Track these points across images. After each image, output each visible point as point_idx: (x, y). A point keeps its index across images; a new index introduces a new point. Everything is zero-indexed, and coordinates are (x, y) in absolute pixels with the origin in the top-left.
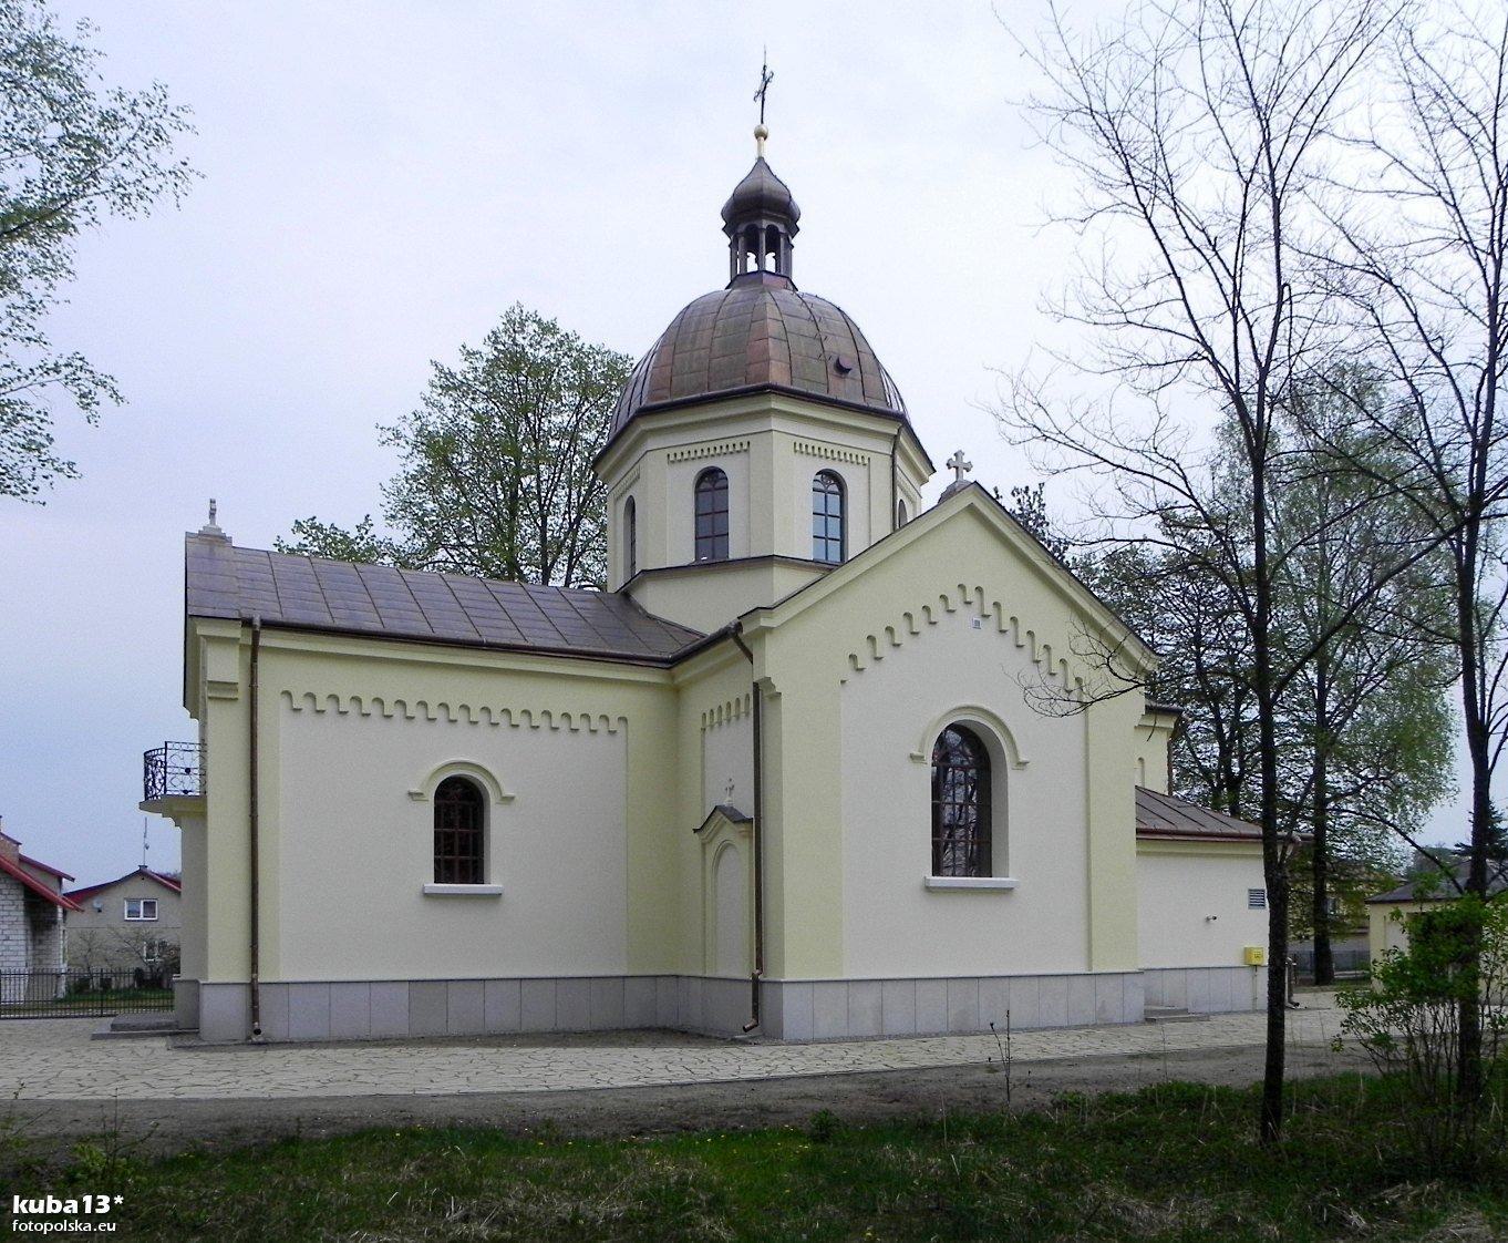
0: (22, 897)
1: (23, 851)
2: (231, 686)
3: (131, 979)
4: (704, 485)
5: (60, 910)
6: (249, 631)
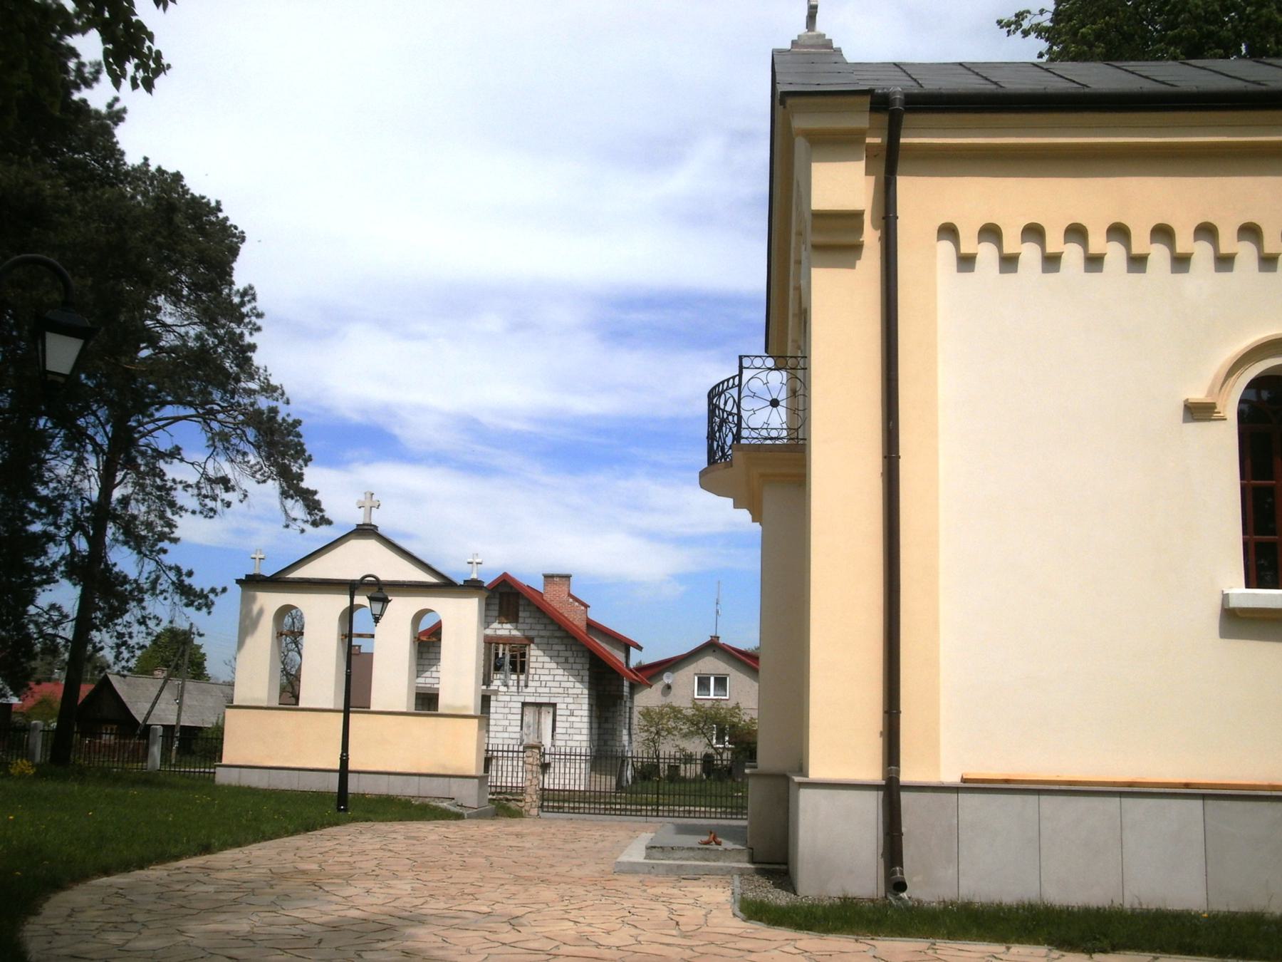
0: (587, 666)
1: (594, 615)
2: (854, 218)
3: (699, 767)
5: (626, 683)
6: (884, 119)
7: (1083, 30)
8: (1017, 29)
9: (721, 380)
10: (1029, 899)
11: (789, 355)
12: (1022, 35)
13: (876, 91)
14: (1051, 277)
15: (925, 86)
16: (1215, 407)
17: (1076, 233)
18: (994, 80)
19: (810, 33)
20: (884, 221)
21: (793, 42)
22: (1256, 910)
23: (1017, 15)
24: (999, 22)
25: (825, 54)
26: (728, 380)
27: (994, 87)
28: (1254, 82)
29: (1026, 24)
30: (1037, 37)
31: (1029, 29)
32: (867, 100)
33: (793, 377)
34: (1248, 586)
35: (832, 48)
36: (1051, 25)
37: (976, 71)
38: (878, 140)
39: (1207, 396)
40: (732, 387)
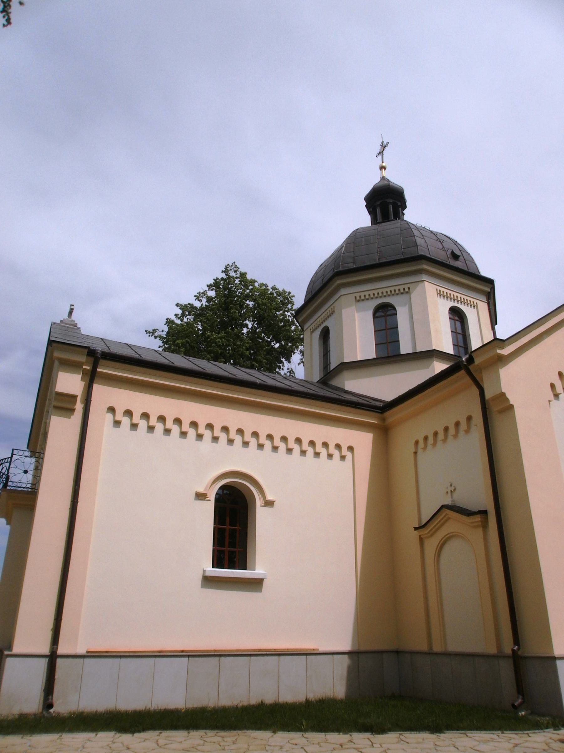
2: (73, 398)
4: (378, 314)
7: (177, 341)
8: (152, 335)
9: (2, 459)
10: (110, 710)
11: (37, 451)
12: (154, 338)
13: (91, 348)
14: (150, 435)
15: (111, 350)
16: (207, 495)
17: (162, 419)
18: (138, 353)
19: (69, 319)
20: (85, 401)
21: (61, 321)
22: (204, 706)
23: (153, 330)
24: (146, 331)
25: (74, 329)
26: (5, 459)
27: (138, 356)
28: (232, 374)
29: (156, 334)
30: (159, 340)
31: (157, 336)
32: (86, 351)
33: (37, 462)
34: (213, 567)
35: (77, 327)
36: (166, 336)
37: (132, 348)
38: (88, 368)
39: (204, 491)
40: (7, 462)
